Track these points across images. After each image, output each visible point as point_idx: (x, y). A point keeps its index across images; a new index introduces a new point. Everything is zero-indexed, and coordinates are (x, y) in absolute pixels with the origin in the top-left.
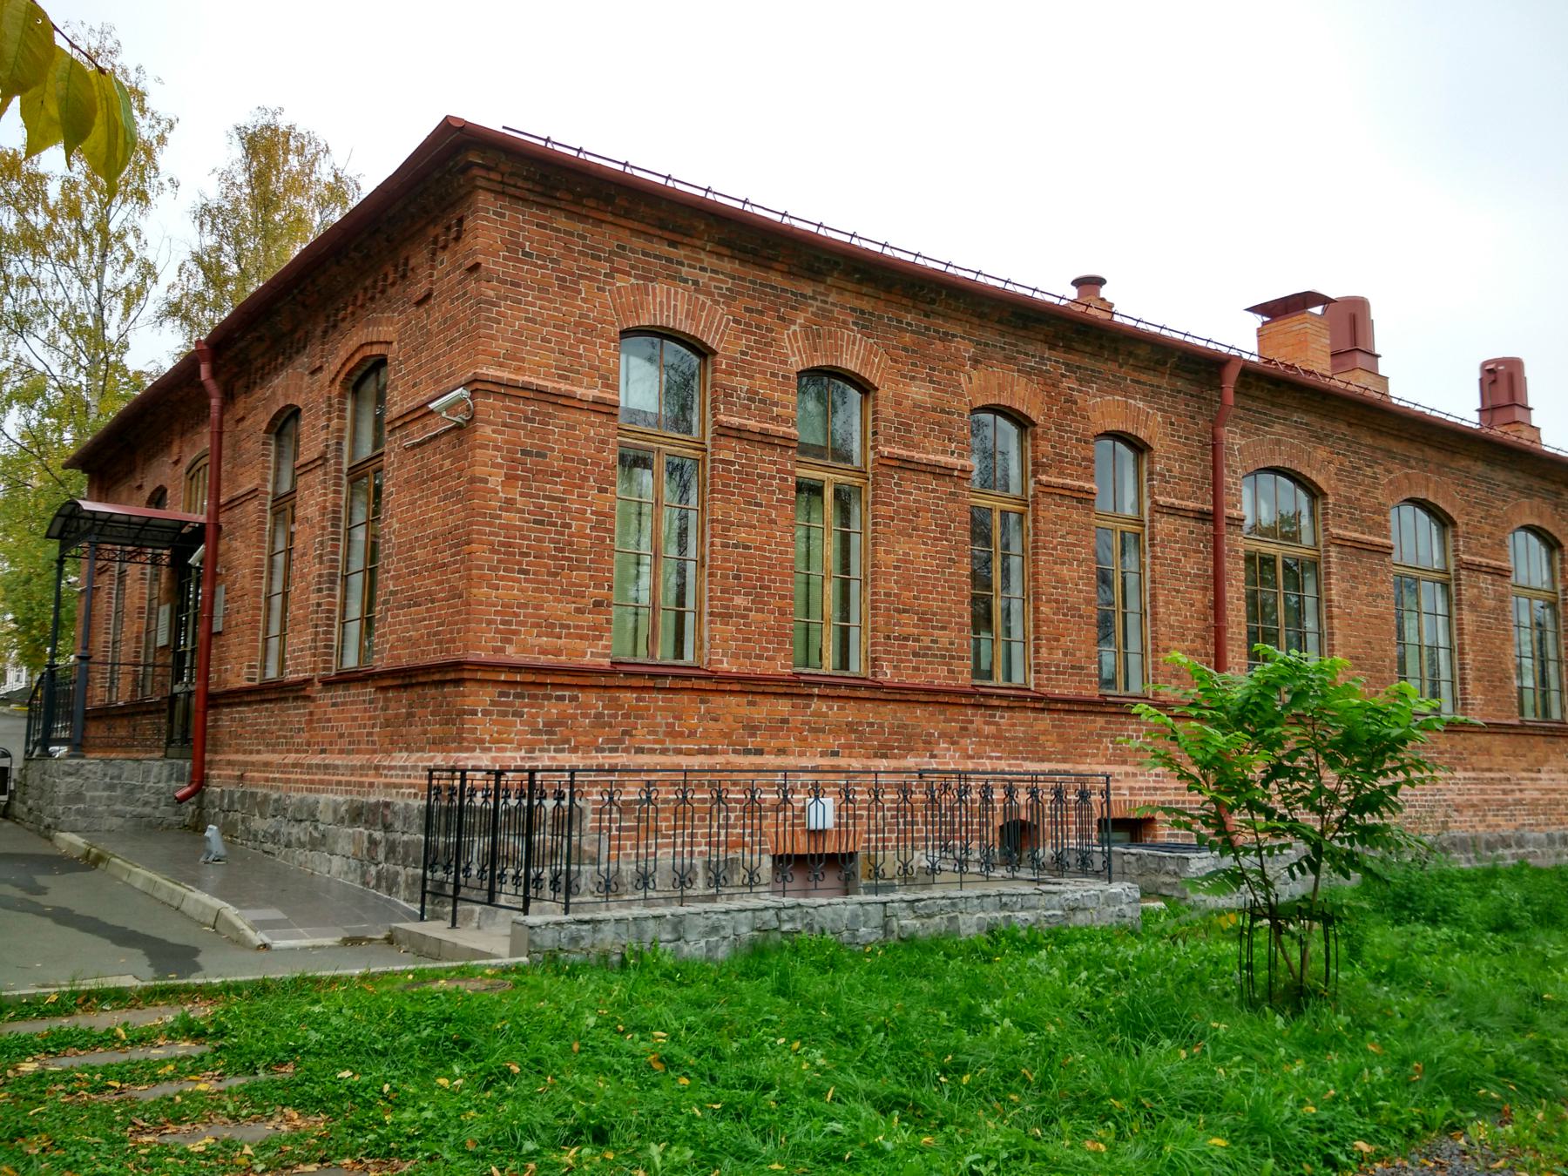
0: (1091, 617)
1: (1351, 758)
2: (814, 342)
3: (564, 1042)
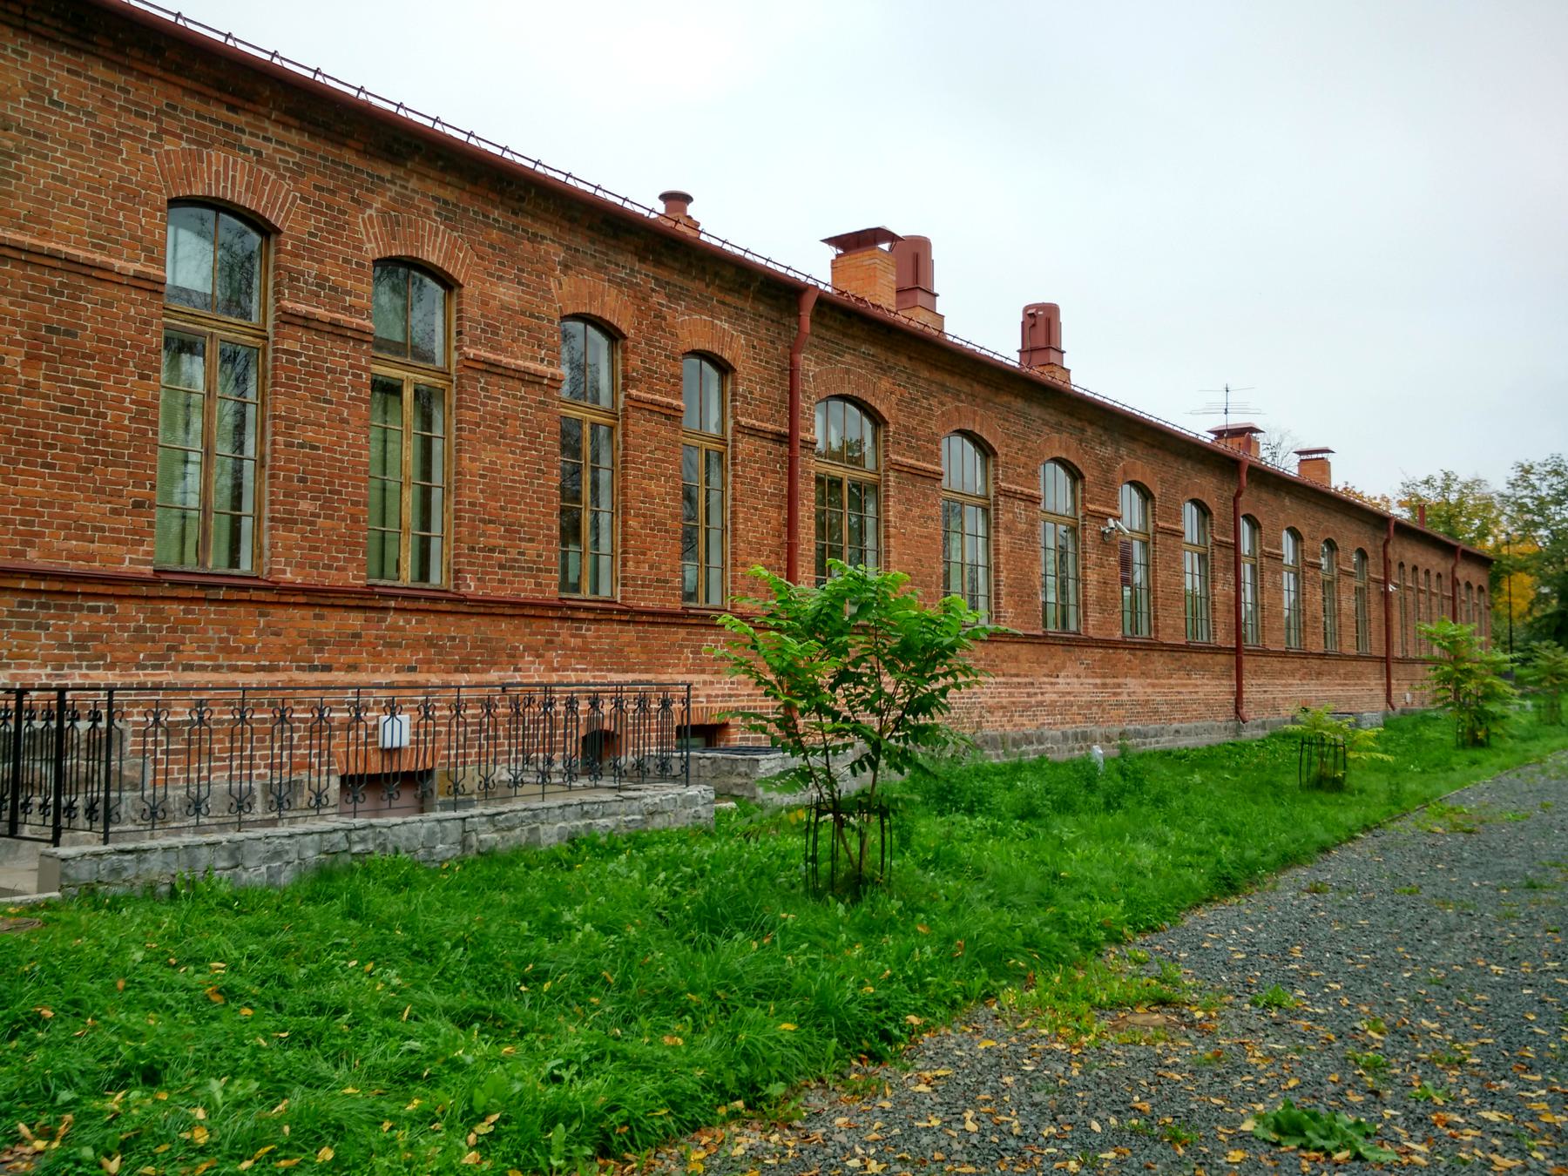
0: (675, 532)
1: (907, 664)
2: (392, 229)
3: (107, 981)
